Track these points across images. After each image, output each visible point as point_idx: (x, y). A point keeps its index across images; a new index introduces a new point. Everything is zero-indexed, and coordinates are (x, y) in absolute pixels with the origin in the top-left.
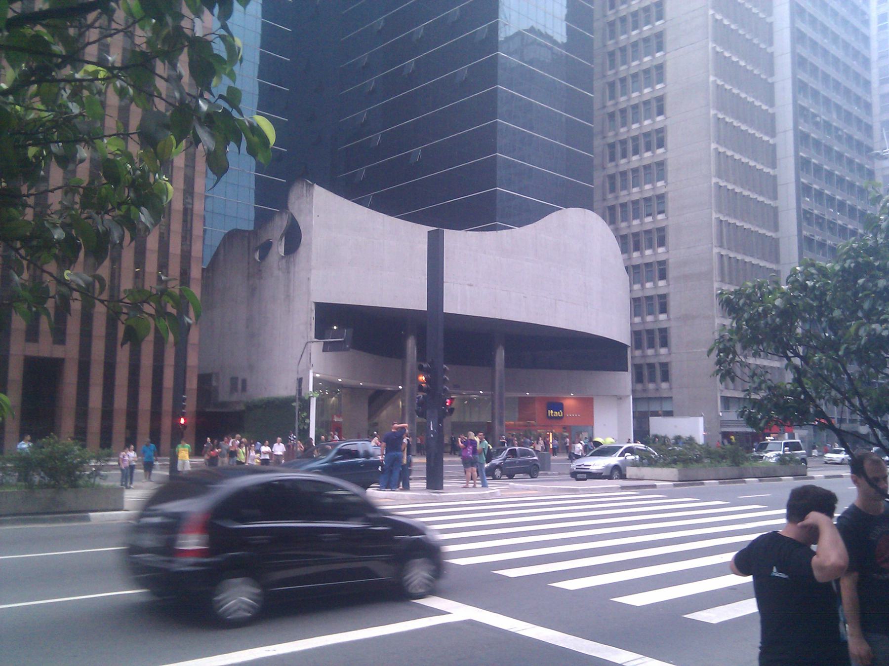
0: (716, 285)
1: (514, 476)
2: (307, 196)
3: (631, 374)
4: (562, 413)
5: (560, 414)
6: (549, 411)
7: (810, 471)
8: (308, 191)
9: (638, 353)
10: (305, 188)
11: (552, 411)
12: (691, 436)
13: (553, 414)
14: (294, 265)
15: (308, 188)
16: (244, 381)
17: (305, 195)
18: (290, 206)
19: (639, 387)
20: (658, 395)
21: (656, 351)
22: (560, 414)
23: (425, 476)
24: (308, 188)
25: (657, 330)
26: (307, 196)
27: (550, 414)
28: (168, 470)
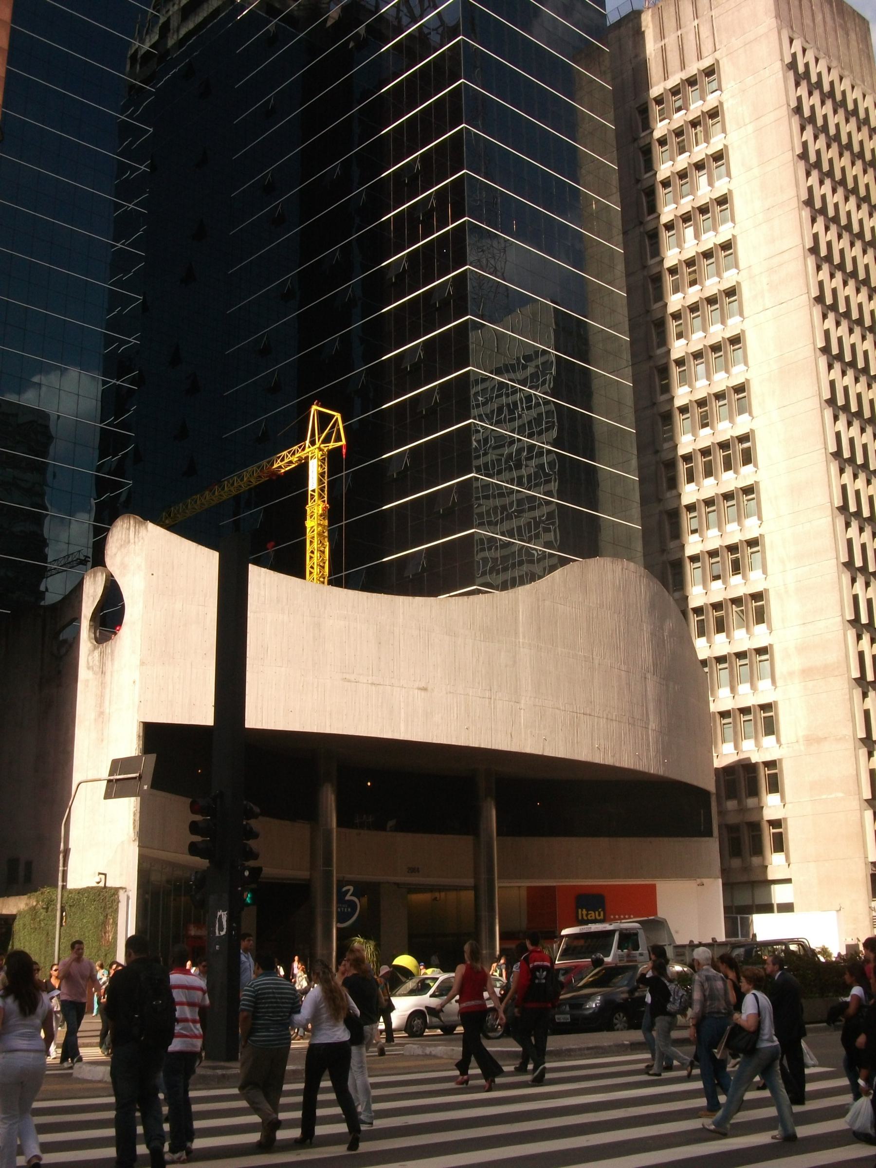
0: (322, 868)
1: (454, 1030)
2: (135, 542)
3: (717, 840)
4: (602, 913)
5: (599, 915)
6: (580, 910)
7: (81, 1037)
8: (137, 533)
9: (731, 805)
10: (132, 529)
11: (584, 910)
12: (824, 946)
13: (587, 915)
14: (112, 660)
15: (137, 527)
16: (29, 864)
17: (132, 541)
18: (108, 561)
19: (736, 863)
20: (745, 878)
21: (740, 802)
22: (599, 915)
23: (807, 1026)
24: (137, 527)
25: (761, 764)
26: (135, 542)
27: (582, 915)
28: (461, 1043)
